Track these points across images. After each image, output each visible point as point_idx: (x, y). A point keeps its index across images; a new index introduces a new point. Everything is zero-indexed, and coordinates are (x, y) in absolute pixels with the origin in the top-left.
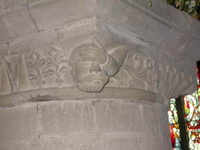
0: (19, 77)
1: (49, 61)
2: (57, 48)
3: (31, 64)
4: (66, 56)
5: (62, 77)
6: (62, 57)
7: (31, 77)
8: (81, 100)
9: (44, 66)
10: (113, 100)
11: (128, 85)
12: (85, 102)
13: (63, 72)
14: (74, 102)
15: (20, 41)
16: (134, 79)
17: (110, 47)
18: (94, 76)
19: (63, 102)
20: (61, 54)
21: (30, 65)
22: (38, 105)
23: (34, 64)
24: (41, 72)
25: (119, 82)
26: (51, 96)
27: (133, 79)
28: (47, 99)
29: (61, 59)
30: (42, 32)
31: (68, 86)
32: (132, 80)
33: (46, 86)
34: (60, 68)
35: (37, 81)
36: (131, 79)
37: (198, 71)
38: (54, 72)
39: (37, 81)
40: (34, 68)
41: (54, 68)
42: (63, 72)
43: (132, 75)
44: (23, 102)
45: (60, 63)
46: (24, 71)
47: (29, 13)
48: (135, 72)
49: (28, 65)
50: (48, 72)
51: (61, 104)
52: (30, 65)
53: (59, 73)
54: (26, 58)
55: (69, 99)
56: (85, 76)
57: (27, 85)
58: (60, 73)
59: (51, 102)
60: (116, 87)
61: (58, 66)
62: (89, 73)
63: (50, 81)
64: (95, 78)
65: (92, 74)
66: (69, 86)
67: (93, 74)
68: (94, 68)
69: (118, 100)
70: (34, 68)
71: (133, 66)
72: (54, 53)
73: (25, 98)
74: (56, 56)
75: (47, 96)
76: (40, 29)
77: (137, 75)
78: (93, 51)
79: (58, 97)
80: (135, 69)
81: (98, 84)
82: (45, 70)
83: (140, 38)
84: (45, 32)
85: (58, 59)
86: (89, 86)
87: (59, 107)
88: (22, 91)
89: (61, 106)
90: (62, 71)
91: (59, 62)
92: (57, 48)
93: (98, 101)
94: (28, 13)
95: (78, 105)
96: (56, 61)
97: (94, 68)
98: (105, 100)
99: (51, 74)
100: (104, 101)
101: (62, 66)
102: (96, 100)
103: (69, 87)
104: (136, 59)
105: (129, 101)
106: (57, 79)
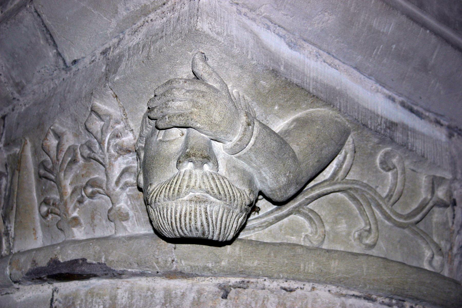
0: (14, 211)
1: (87, 152)
2: (106, 108)
3: (45, 168)
5: (126, 203)
6: (117, 136)
7: (45, 209)
8: (185, 281)
9: (75, 168)
10: (292, 284)
11: (355, 243)
12: (196, 288)
14: (162, 284)
15: (27, 106)
16: (376, 223)
18: (187, 178)
19: (128, 285)
20: (118, 126)
21: (42, 172)
22: (55, 294)
23: (50, 166)
24: (69, 190)
25: (320, 231)
26: (89, 261)
27: (373, 227)
28: (78, 270)
29: (118, 140)
30: (74, 68)
32: (369, 231)
33: (79, 234)
34: (116, 173)
35: (59, 218)
36: (368, 227)
37: (430, 32)
38: (102, 188)
40: (51, 180)
41: (99, 175)
44: (15, 282)
45: (116, 159)
47: (36, 11)
48: (384, 207)
50: (85, 188)
51: (119, 291)
52: (42, 172)
53: (114, 190)
54: (35, 153)
55: (142, 274)
56: (164, 180)
57: (35, 234)
58: (118, 189)
59: (94, 282)
60: (308, 244)
61: (111, 164)
62: (176, 171)
63: (93, 218)
64: (192, 184)
67: (185, 171)
68: (188, 150)
69: (313, 288)
70: (51, 180)
71: (378, 190)
72: (97, 125)
73: (18, 269)
74: (102, 132)
75: (76, 261)
76: (69, 61)
77: (389, 218)
78: (188, 94)
79: (107, 265)
81: (203, 206)
82: (79, 184)
83: (403, 104)
84: (80, 66)
85: (109, 143)
86: (176, 213)
87: (114, 298)
88: (19, 252)
89: (119, 297)
90: (123, 182)
91: (112, 152)
92: (106, 108)
93: (242, 286)
94: (33, 10)
95: (173, 295)
96: (103, 151)
97: (188, 150)
98: (267, 283)
99: (92, 196)
100: (264, 289)
101: (124, 166)
102: (233, 280)
104: (386, 165)
105: (353, 295)
106: (110, 211)
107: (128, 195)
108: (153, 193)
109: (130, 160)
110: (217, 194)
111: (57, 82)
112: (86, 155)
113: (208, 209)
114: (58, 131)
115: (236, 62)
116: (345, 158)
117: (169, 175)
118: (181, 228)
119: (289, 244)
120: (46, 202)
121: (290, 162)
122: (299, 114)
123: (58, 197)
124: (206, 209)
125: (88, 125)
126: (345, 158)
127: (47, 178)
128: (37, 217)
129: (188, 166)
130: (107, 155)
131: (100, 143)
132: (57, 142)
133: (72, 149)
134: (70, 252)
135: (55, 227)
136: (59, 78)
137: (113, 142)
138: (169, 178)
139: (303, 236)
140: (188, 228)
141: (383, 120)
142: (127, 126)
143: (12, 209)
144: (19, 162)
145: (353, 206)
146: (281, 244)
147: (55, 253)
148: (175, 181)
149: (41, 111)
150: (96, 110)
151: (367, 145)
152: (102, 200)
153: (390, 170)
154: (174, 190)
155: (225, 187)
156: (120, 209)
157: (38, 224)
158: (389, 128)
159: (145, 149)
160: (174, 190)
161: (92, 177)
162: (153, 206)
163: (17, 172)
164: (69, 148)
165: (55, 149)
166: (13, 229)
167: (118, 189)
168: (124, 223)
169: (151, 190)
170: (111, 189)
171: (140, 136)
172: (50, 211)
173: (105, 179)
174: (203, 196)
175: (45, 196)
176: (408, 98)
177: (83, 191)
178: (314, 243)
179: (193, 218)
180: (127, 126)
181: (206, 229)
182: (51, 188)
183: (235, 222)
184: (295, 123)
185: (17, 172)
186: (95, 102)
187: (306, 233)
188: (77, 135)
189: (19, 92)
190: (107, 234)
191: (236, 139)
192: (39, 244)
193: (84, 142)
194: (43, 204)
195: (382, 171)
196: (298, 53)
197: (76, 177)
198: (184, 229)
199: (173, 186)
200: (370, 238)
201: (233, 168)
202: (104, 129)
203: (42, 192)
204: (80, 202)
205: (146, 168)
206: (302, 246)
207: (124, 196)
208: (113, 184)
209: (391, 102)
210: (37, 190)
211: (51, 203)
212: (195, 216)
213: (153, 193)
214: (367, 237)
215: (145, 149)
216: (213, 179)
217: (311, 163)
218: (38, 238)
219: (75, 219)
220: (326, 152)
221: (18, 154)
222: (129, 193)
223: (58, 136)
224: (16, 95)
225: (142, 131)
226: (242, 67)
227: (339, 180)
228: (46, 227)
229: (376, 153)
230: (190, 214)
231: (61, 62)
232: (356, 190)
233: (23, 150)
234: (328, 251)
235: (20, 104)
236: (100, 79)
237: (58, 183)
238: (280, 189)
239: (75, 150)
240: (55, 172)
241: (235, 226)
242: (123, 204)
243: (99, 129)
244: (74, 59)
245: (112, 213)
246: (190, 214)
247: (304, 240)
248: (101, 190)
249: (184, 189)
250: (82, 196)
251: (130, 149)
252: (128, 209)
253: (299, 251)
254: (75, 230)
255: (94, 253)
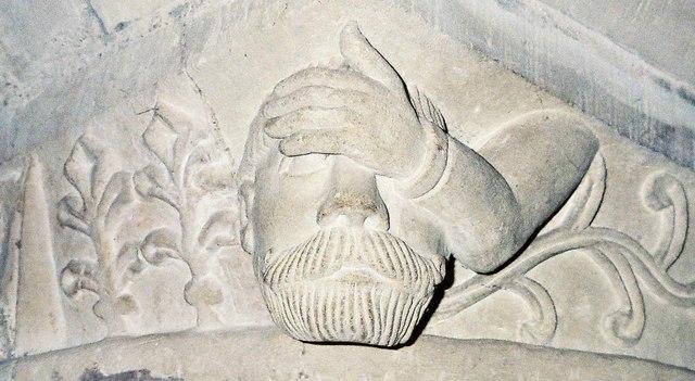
0: (15, 283)
1: (146, 185)
3: (70, 210)
4: (225, 156)
7: (69, 280)
9: (125, 210)
11: (607, 336)
13: (218, 243)
17: (477, 110)
18: (336, 241)
20: (202, 142)
21: (65, 216)
23: (79, 208)
24: (115, 250)
27: (637, 308)
29: (203, 167)
30: (119, 36)
31: (245, 324)
32: (630, 314)
34: (200, 222)
35: (97, 297)
38: (174, 247)
39: (97, 297)
40: (82, 231)
41: (169, 224)
42: (218, 243)
43: (629, 284)
45: (199, 197)
46: (42, 248)
48: (653, 271)
49: (58, 218)
50: (143, 247)
52: (65, 216)
54: (50, 181)
56: (294, 245)
58: (203, 251)
60: (528, 340)
62: (316, 228)
63: (157, 299)
64: (346, 252)
65: (328, 229)
66: (252, 323)
68: (338, 195)
70: (82, 231)
71: (642, 242)
72: (164, 139)
76: (110, 24)
77: (662, 291)
80: (651, 258)
81: (364, 290)
82: (132, 240)
83: (683, 94)
84: (131, 33)
85: (186, 171)
91: (193, 184)
97: (338, 195)
99: (157, 259)
101: (212, 211)
103: (250, 329)
104: (657, 196)
107: (220, 261)
108: (275, 267)
109: (226, 200)
110: (390, 269)
111: (87, 59)
112: (145, 191)
113: (372, 294)
114: (94, 146)
115: (414, 36)
116: (589, 190)
117: (303, 237)
118: (325, 327)
119: (496, 342)
120: (72, 268)
121: (504, 206)
122: (516, 119)
123: (94, 261)
124: (369, 294)
125: (149, 138)
126: (589, 190)
127: (74, 228)
128: (57, 294)
129: (338, 221)
130: (184, 192)
131: (171, 172)
132: (91, 165)
133: (120, 177)
134: (120, 358)
135: (91, 311)
136: (91, 52)
137: (196, 169)
138: (303, 242)
139: (519, 326)
140: (338, 328)
141: (653, 123)
142: (219, 142)
143: (11, 279)
144: (23, 198)
145: (602, 271)
146: (484, 341)
147: (94, 359)
148: (315, 247)
149: (59, 109)
150: (164, 114)
151: (624, 166)
152: (174, 267)
153: (663, 207)
154: (314, 262)
155: (401, 257)
156: (206, 283)
157: (58, 308)
158: (662, 137)
159: (257, 184)
160: (314, 262)
161: (156, 227)
162: (275, 287)
163: (18, 215)
164: (115, 176)
165: (88, 178)
166: (13, 314)
167: (203, 251)
168: (214, 308)
169: (271, 262)
170: (191, 250)
171: (245, 161)
172: (80, 285)
173: (179, 231)
174: (363, 272)
175: (70, 259)
176: (691, 81)
177: (140, 252)
178: (539, 338)
179: (346, 310)
180: (219, 142)
181: (369, 328)
182: (81, 245)
183: (416, 314)
184: (508, 136)
185: (18, 215)
186: (162, 100)
187: (524, 321)
188: (127, 154)
189: (17, 74)
190: (184, 325)
191: (419, 171)
192: (59, 343)
193: (140, 167)
194: (67, 272)
195: (649, 209)
196: (514, 15)
197: (127, 227)
198: (330, 328)
199: (312, 256)
200: (630, 327)
201: (413, 223)
202: (178, 147)
203: (64, 248)
204: (134, 270)
205: (260, 219)
206: (519, 345)
207: (213, 261)
208: (195, 242)
209: (664, 90)
210: (55, 245)
211: (82, 272)
212: (351, 307)
213: (275, 267)
214: (626, 325)
215: (257, 184)
216: (382, 243)
217: (537, 205)
218: (59, 332)
219: (126, 299)
220: (561, 186)
221: (18, 182)
222: (221, 257)
223: (95, 155)
224: (12, 78)
225: (248, 151)
226: (423, 45)
227: (580, 229)
228: (74, 312)
229: (639, 180)
230: (342, 303)
231: (96, 25)
232: (608, 244)
233: (27, 176)
234: (562, 352)
235: (18, 93)
236: (170, 62)
237: (96, 238)
238: (487, 253)
239: (124, 182)
240: (88, 217)
241: (414, 319)
242: (212, 273)
243: (170, 147)
244: (119, 22)
245: (193, 289)
246: (342, 303)
247: (521, 335)
248: (173, 252)
249: (332, 262)
250: (139, 260)
251: (224, 183)
252: (219, 282)
253: (516, 353)
254: (126, 318)
255: (161, 362)
